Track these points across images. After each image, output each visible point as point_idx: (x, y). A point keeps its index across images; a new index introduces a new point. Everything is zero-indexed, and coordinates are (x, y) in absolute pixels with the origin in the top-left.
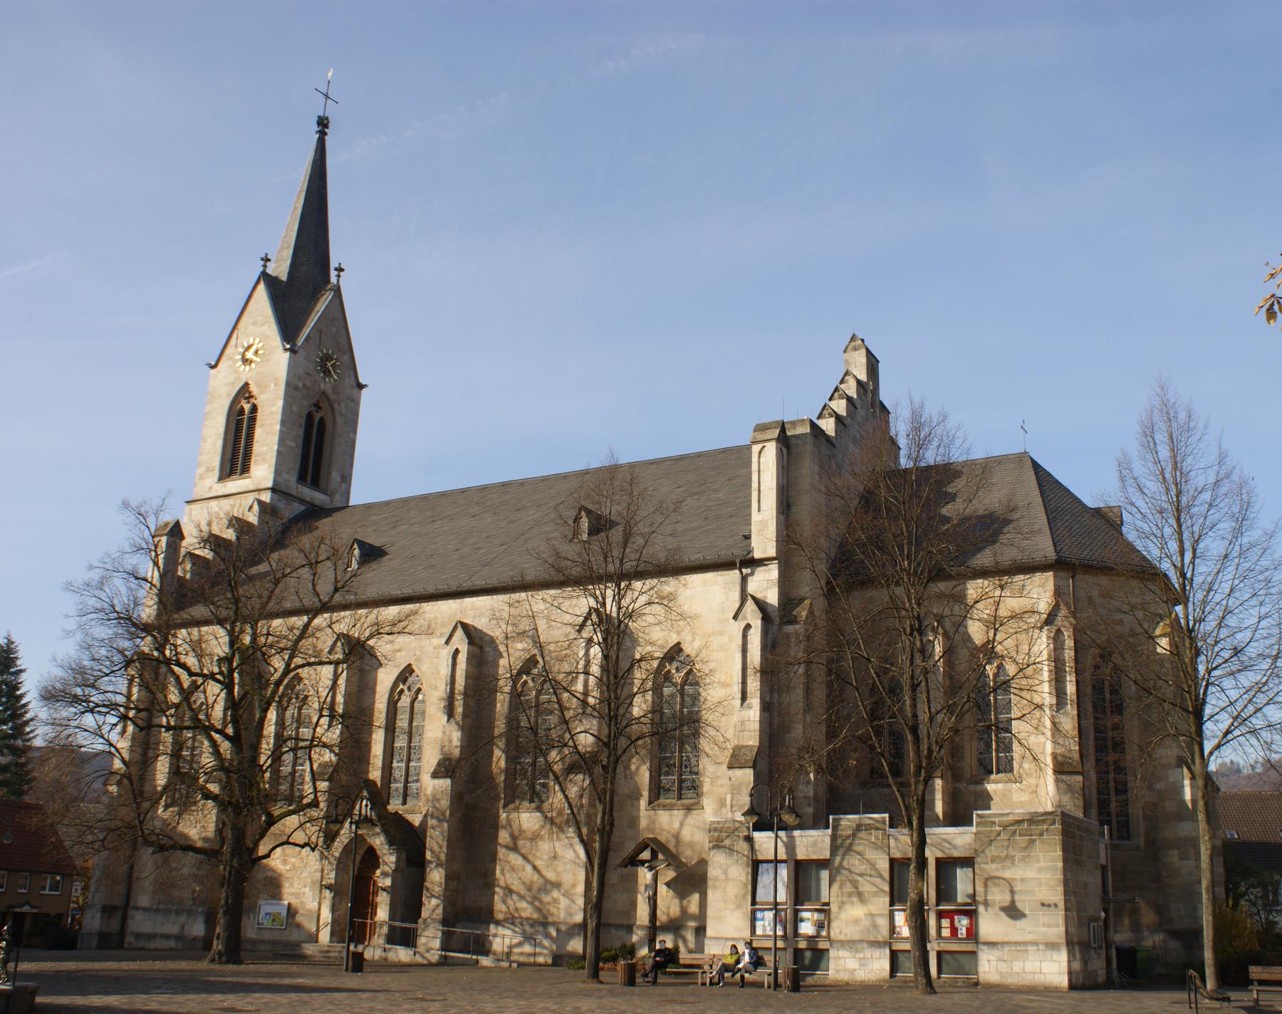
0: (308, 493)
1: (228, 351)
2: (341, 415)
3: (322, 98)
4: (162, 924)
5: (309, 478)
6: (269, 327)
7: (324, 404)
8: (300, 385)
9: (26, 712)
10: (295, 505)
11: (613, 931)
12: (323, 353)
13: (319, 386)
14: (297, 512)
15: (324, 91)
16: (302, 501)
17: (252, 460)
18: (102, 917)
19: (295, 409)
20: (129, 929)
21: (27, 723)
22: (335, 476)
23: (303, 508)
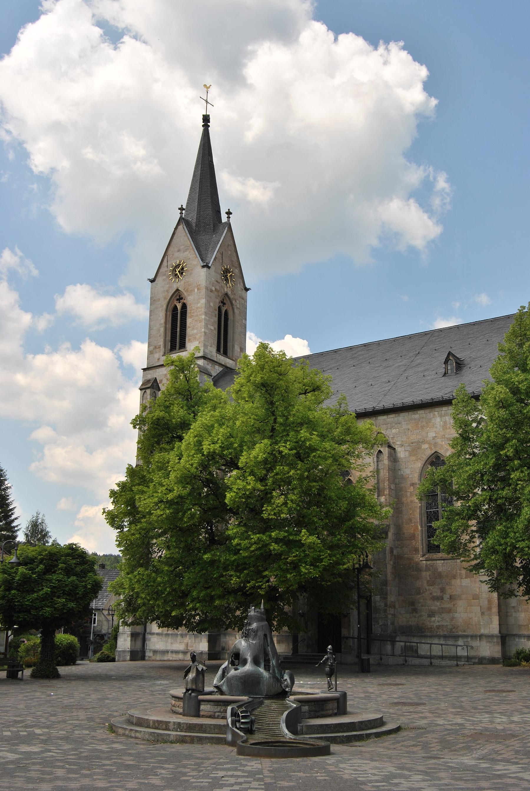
0: (222, 359)
1: (161, 270)
2: (237, 308)
3: (208, 100)
4: (172, 644)
5: (222, 350)
6: (190, 252)
7: (227, 301)
8: (213, 289)
9: (12, 514)
10: (217, 367)
11: (517, 640)
12: (225, 268)
13: (224, 289)
14: (218, 372)
15: (205, 99)
16: (220, 365)
17: (187, 339)
18: (131, 640)
19: (212, 304)
20: (148, 648)
21: (13, 521)
22: (237, 348)
23: (221, 369)
